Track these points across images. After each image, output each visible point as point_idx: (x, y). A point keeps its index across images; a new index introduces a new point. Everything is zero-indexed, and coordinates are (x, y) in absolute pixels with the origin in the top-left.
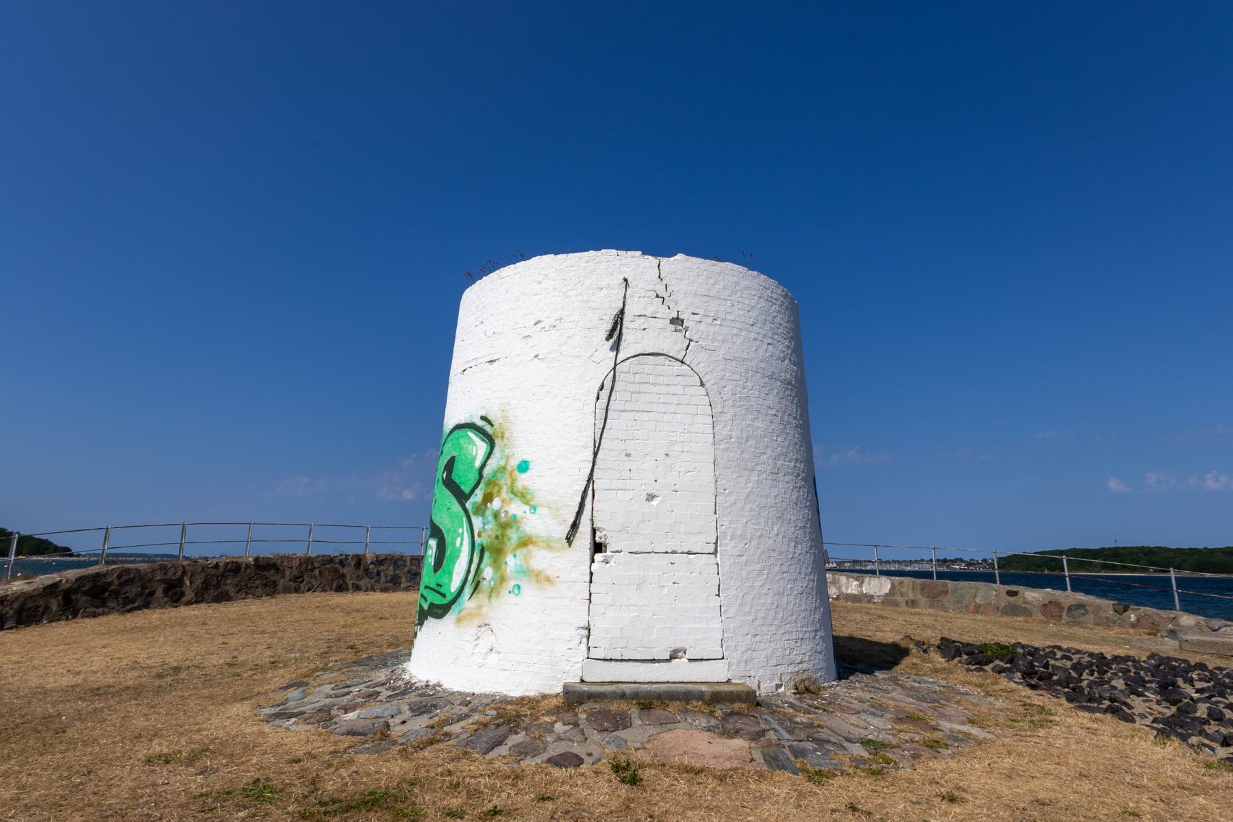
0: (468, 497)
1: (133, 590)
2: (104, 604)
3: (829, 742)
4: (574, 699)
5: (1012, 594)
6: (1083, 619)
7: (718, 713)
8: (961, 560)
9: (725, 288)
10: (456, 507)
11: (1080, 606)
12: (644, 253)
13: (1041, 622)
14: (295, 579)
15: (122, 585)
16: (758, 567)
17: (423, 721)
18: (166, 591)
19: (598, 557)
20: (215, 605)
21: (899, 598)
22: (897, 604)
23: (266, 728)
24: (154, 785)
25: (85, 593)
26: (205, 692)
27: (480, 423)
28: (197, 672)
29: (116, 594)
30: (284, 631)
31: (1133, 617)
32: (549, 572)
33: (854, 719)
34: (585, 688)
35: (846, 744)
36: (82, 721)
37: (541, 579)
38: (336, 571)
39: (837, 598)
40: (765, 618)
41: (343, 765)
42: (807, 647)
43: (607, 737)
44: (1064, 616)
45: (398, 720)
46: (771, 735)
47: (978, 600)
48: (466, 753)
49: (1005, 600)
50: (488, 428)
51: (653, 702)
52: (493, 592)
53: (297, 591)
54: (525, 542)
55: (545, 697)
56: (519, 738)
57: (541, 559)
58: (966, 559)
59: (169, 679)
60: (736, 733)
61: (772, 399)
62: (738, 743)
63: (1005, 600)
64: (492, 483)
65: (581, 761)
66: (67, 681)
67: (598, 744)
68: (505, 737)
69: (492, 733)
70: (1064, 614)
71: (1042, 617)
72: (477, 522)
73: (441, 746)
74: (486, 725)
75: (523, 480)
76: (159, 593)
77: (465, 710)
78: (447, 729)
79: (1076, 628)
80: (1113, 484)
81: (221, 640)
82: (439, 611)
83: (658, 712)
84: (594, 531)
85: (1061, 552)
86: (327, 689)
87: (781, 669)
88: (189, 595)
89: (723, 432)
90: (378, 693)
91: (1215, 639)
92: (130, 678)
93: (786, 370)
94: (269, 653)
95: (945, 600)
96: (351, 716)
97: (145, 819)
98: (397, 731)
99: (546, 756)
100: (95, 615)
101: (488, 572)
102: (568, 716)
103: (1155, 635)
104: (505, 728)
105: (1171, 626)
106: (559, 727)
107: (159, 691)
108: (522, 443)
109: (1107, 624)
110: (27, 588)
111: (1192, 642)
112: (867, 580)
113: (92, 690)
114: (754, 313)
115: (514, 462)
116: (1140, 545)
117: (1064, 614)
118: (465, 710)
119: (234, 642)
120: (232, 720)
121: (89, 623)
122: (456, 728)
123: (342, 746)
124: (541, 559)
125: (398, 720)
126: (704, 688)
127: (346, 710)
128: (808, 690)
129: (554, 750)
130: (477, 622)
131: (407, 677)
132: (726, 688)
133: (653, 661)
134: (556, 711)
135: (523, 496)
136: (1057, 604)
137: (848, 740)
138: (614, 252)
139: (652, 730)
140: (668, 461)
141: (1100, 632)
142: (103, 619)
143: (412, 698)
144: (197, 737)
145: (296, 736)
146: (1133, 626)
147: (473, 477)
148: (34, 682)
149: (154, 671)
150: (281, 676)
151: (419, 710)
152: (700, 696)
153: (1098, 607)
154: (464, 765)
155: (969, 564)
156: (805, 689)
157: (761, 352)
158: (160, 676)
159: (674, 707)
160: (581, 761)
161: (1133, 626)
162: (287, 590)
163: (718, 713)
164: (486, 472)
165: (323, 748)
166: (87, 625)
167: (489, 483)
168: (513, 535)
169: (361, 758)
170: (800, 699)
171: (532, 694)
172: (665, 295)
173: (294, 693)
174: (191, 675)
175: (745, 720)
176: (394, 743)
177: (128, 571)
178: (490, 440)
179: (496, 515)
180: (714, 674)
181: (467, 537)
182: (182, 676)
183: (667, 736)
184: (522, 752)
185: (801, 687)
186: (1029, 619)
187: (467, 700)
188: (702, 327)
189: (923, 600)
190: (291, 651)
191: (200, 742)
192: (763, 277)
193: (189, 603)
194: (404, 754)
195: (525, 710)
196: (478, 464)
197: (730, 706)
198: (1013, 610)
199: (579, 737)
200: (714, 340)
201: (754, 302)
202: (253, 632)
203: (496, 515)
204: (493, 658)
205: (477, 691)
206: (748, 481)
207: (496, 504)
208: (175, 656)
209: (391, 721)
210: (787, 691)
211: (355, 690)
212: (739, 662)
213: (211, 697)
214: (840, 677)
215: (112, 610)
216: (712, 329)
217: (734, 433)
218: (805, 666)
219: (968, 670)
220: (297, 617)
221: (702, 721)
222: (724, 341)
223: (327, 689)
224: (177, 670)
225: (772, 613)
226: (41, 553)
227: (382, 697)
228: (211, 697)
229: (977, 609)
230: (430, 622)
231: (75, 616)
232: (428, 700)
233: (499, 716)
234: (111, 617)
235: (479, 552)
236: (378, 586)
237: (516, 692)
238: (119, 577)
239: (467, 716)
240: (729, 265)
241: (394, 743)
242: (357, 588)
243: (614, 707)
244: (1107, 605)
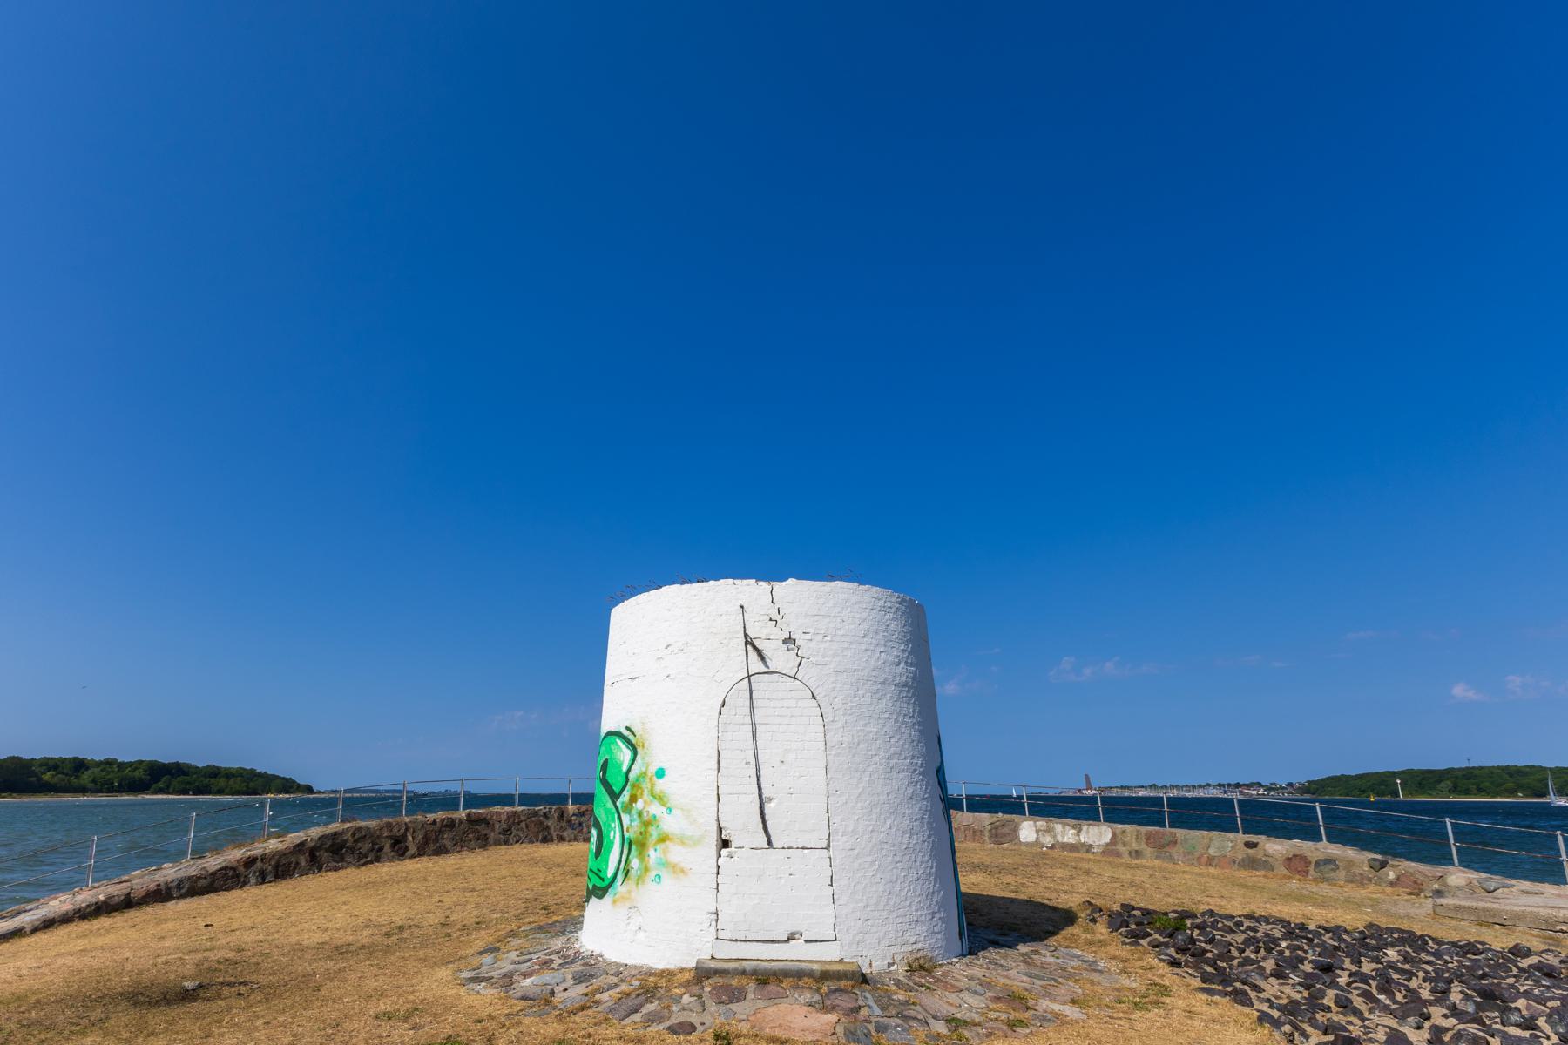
0: (618, 797)
1: (365, 847)
2: (342, 859)
3: (915, 1018)
4: (702, 974)
5: (1249, 845)
6: (1333, 875)
7: (825, 989)
8: (1259, 785)
9: (835, 606)
10: (610, 805)
11: (1330, 861)
12: (758, 579)
13: (1284, 877)
14: (504, 832)
15: (356, 842)
16: (869, 859)
18: (393, 846)
19: (724, 852)
20: (435, 858)
21: (1120, 848)
22: (1118, 855)
23: (462, 991)
24: (380, 1037)
25: (327, 850)
26: (421, 953)
27: (626, 733)
28: (416, 931)
29: (352, 850)
30: (490, 889)
31: (1392, 875)
32: (683, 865)
33: (952, 998)
34: (713, 965)
35: (931, 1021)
36: (331, 980)
37: (677, 870)
38: (541, 823)
39: (1053, 847)
40: (877, 904)
41: (513, 1025)
42: (922, 929)
43: (722, 1008)
44: (1312, 872)
46: (864, 1012)
47: (1211, 851)
48: (607, 1019)
49: (1242, 853)
50: (631, 737)
51: (768, 978)
52: (639, 879)
53: (506, 843)
54: (663, 839)
55: (682, 970)
57: (676, 853)
58: (1266, 782)
59: (394, 938)
60: (833, 1008)
61: (885, 703)
62: (831, 1018)
63: (1242, 853)
64: (635, 786)
66: (317, 938)
67: (712, 1015)
68: (641, 1006)
69: (632, 1002)
70: (1312, 868)
71: (1285, 872)
72: (625, 818)
73: (590, 1012)
74: (628, 995)
75: (661, 785)
76: (387, 848)
77: (616, 980)
78: (598, 997)
79: (1324, 886)
80: (1459, 691)
81: (437, 898)
82: (600, 892)
83: (772, 988)
84: (720, 829)
85: (1394, 774)
86: (513, 955)
87: (893, 949)
88: (413, 850)
89: (833, 738)
90: (552, 961)
91: (1475, 904)
92: (365, 937)
93: (902, 673)
94: (476, 913)
95: (1174, 851)
96: (528, 981)
97: (402, 1032)
98: (560, 996)
99: (668, 1024)
101: (635, 863)
102: (695, 989)
103: (1418, 895)
105: (1436, 886)
106: (686, 999)
107: (387, 950)
108: (657, 754)
109: (1361, 881)
110: (281, 847)
111: (1447, 907)
112: (1085, 828)
113: (337, 948)
114: (865, 626)
115: (652, 770)
116: (1521, 762)
117: (1312, 868)
118: (616, 980)
119: (449, 900)
120: (437, 983)
121: (332, 876)
122: (604, 997)
123: (516, 1009)
124: (676, 853)
125: (561, 988)
126: (816, 967)
127: (525, 976)
128: (922, 967)
129: (675, 1020)
131: (577, 946)
132: (835, 967)
133: (773, 942)
135: (660, 799)
136: (1303, 859)
137: (935, 1017)
138: (731, 581)
139: (760, 1004)
140: (784, 767)
141: (1352, 891)
143: (577, 967)
144: (411, 997)
145: (484, 998)
146: (1392, 884)
147: (622, 780)
148: (294, 939)
149: (384, 929)
151: (580, 979)
152: (811, 974)
154: (601, 1030)
155: (1269, 789)
156: (920, 967)
157: (872, 661)
158: (388, 935)
159: (787, 983)
160: (694, 1028)
161: (1392, 884)
162: (498, 843)
163: (825, 989)
164: (631, 776)
165: (500, 1010)
166: (330, 879)
167: (635, 786)
168: (654, 833)
169: (527, 1021)
170: (909, 978)
171: (672, 967)
172: (778, 618)
173: (487, 959)
174: (411, 934)
176: (555, 1008)
177: (360, 829)
178: (634, 748)
179: (640, 814)
181: (618, 830)
182: (405, 935)
183: (770, 1010)
184: (652, 1019)
185: (916, 965)
186: (1270, 874)
187: (619, 971)
188: (812, 645)
189: (1148, 851)
190: (493, 911)
191: (414, 1002)
192: (875, 589)
193: (413, 857)
194: (560, 1018)
195: (662, 983)
196: (625, 769)
197: (839, 984)
198: (1252, 864)
199: (699, 1008)
200: (824, 656)
201: (864, 615)
202: (465, 890)
203: (640, 814)
204: (641, 935)
207: (639, 805)
208: (400, 915)
209: (556, 989)
210: (900, 970)
211: (534, 956)
212: (850, 944)
213: (425, 960)
214: (972, 952)
216: (823, 646)
217: (846, 739)
218: (919, 946)
219: (1124, 943)
220: (504, 873)
221: (807, 996)
222: (834, 656)
223: (513, 955)
224: (401, 928)
225: (884, 900)
226: (287, 792)
227: (554, 965)
228: (425, 960)
229: (1210, 861)
230: (594, 900)
231: (320, 870)
232: (589, 970)
234: (349, 871)
235: (628, 844)
236: (580, 837)
237: (660, 965)
238: (353, 835)
239: (616, 985)
241: (555, 1008)
242: (561, 839)
243: (735, 982)
244: (1360, 858)
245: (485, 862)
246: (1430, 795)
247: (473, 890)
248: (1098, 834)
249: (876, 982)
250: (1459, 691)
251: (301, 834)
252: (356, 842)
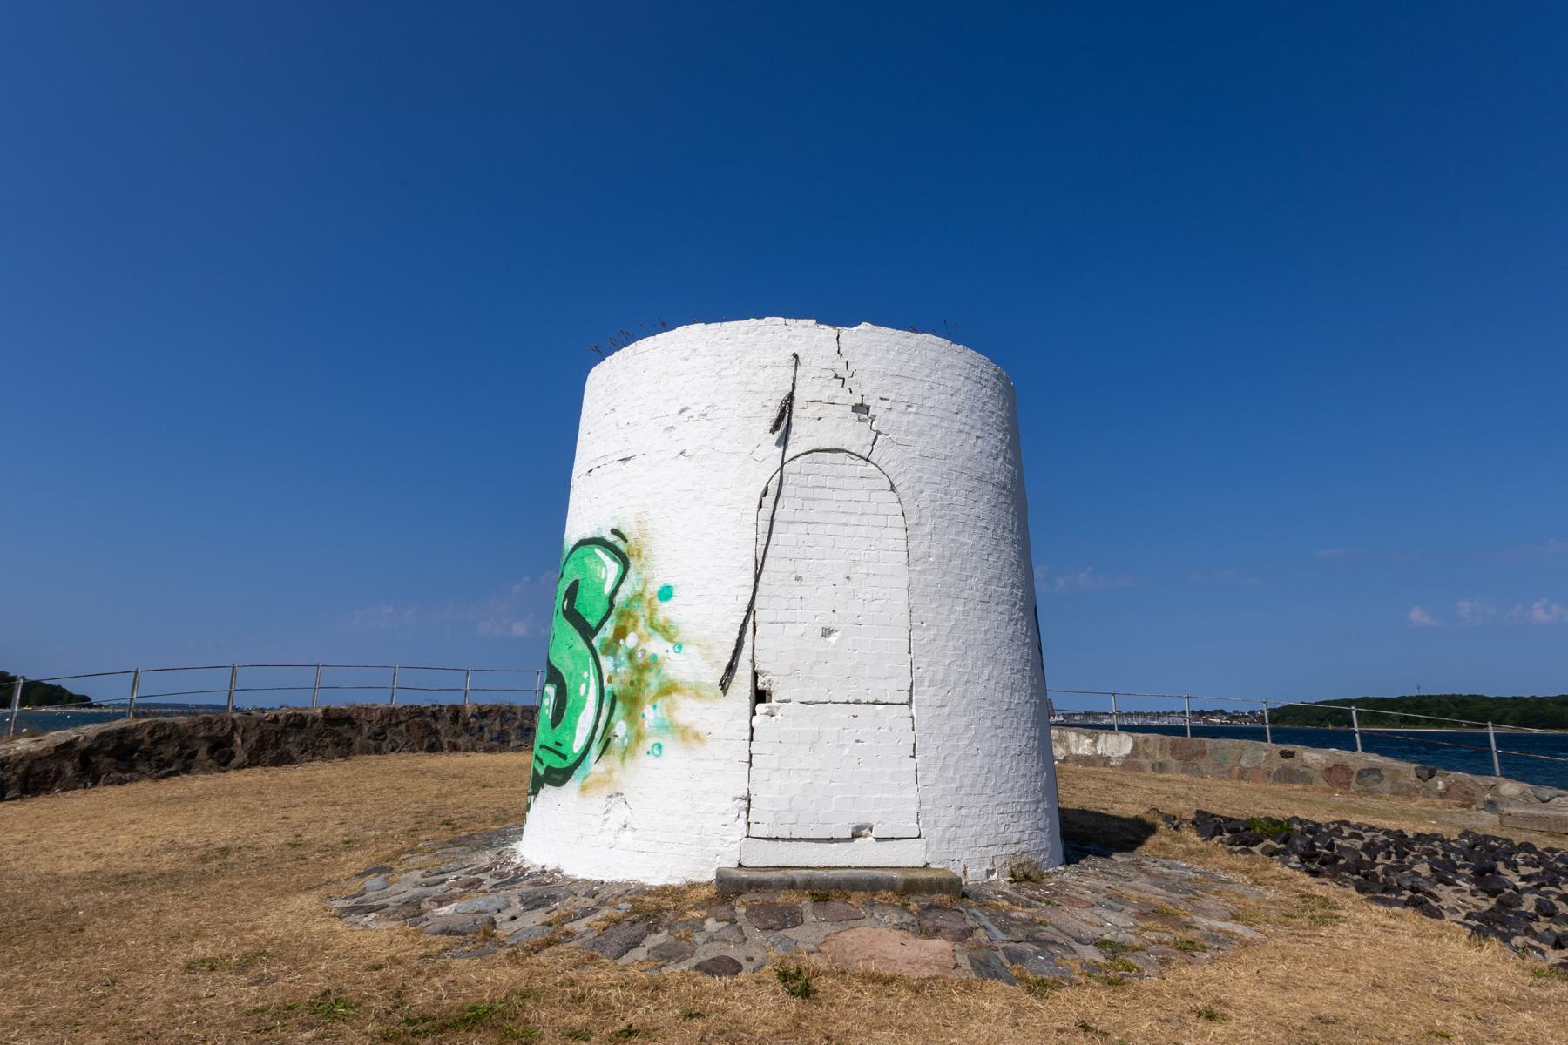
0: (595, 632)
1: (169, 751)
2: (132, 768)
3: (1054, 943)
4: (729, 888)
5: (1286, 755)
6: (1377, 786)
7: (914, 906)
8: (1223, 712)
9: (922, 366)
10: (580, 645)
11: (1374, 770)
12: (819, 322)
13: (1324, 790)
14: (375, 736)
15: (155, 743)
16: (964, 721)
17: (539, 916)
18: (211, 752)
19: (761, 708)
20: (274, 770)
21: (1142, 760)
22: (1140, 768)
23: (339, 926)
24: (196, 998)
25: (108, 754)
27: (611, 538)
28: (250, 855)
29: (148, 755)
30: (361, 802)
32: (698, 728)
33: (1086, 914)
34: (744, 874)
35: (1076, 946)
36: (105, 916)
37: (688, 736)
38: (428, 725)
39: (1065, 761)
40: (973, 785)
41: (436, 972)
42: (1026, 822)
43: (773, 937)
44: (1354, 783)
45: (506, 915)
46: (981, 935)
47: (1243, 763)
48: (592, 957)
49: (1278, 763)
50: (620, 544)
51: (830, 892)
52: (627, 752)
53: (378, 751)
54: (668, 690)
56: (660, 938)
57: (687, 711)
58: (1229, 710)
59: (214, 864)
60: (936, 932)
61: (982, 508)
62: (939, 944)
63: (1278, 763)
64: (626, 614)
65: (739, 968)
66: (85, 865)
67: (760, 945)
68: (642, 937)
69: (626, 932)
70: (1354, 780)
71: (1325, 785)
72: (607, 663)
73: (561, 948)
74: (617, 922)
75: (665, 610)
76: (202, 754)
77: (591, 902)
78: (568, 926)
79: (1369, 799)
80: (1416, 616)
81: (281, 814)
82: (558, 777)
83: (836, 905)
84: (755, 675)
85: (1349, 702)
86: (416, 876)
87: (994, 851)
88: (241, 756)
89: (919, 549)
90: (481, 881)
91: (1545, 813)
92: (166, 862)
93: (1000, 470)
94: (342, 830)
96: (447, 910)
97: (185, 1041)
98: (504, 929)
99: (694, 961)
100: (121, 782)
101: (620, 727)
102: (723, 911)
103: (1469, 807)
104: (642, 926)
105: (1489, 796)
106: (711, 925)
107: (202, 878)
108: (663, 563)
109: (1408, 793)
110: (34, 747)
111: (1516, 817)
112: (1102, 737)
113: (117, 877)
114: (959, 398)
115: (654, 588)
117: (1354, 780)
119: (297, 816)
120: (295, 915)
121: (113, 792)
122: (580, 926)
123: (435, 949)
124: (687, 711)
125: (506, 915)
126: (895, 875)
127: (440, 902)
128: (1027, 877)
130: (606, 791)
131: (517, 861)
132: (923, 875)
133: (831, 840)
134: (707, 904)
135: (665, 631)
136: (1344, 768)
137: (1079, 941)
138: (781, 320)
139: (829, 928)
140: (850, 586)
141: (1399, 803)
142: (131, 787)
143: (524, 887)
144: (250, 937)
145: (377, 935)
146: (1441, 795)
147: (602, 606)
148: (44, 868)
149: (196, 854)
150: (358, 860)
151: (533, 903)
152: (890, 885)
153: (1397, 772)
154: (590, 972)
155: (1232, 717)
156: (1024, 876)
157: (967, 448)
158: (203, 859)
159: (857, 898)
160: (739, 968)
161: (1441, 795)
162: (365, 751)
163: (914, 906)
164: (618, 599)
165: (411, 951)
167: (622, 614)
168: (653, 680)
169: (459, 964)
170: (1017, 889)
171: (676, 882)
172: (846, 375)
173: (374, 882)
174: (242, 858)
175: (947, 915)
176: (501, 944)
177: (162, 726)
178: (624, 560)
179: (631, 655)
180: (908, 856)
182: (231, 859)
183: (848, 936)
184: (664, 956)
185: (1019, 873)
186: (1309, 787)
187: (593, 890)
188: (893, 415)
189: (1173, 763)
190: (370, 828)
191: (254, 944)
192: (970, 352)
193: (240, 767)
194: (514, 958)
195: (668, 903)
196: (607, 590)
197: (928, 898)
198: (1288, 776)
199: (737, 937)
200: (907, 433)
201: (959, 384)
202: (322, 804)
203: (631, 655)
204: (627, 836)
206: (951, 611)
207: (631, 641)
208: (223, 834)
209: (497, 917)
210: (1000, 879)
211: (452, 877)
212: (940, 842)
213: (269, 887)
214: (1068, 860)
215: (142, 776)
216: (906, 419)
217: (934, 551)
218: (1024, 846)
219: (1231, 852)
220: (377, 784)
221: (893, 917)
222: (921, 434)
223: (416, 876)
224: (225, 851)
225: (982, 779)
227: (486, 886)
228: (269, 887)
229: (1243, 775)
230: (547, 791)
231: (95, 783)
232: (544, 890)
233: (635, 910)
234: (141, 784)
235: (609, 701)
236: (480, 745)
238: (152, 733)
239: (594, 910)
240: (927, 337)
241: (501, 944)
242: (454, 748)
243: (780, 899)
244: (1407, 770)
245: (347, 773)
246: (1384, 725)
247: (334, 804)
248: (1117, 746)
249: (977, 897)
250: (1416, 616)
251: (69, 732)
252: (155, 743)
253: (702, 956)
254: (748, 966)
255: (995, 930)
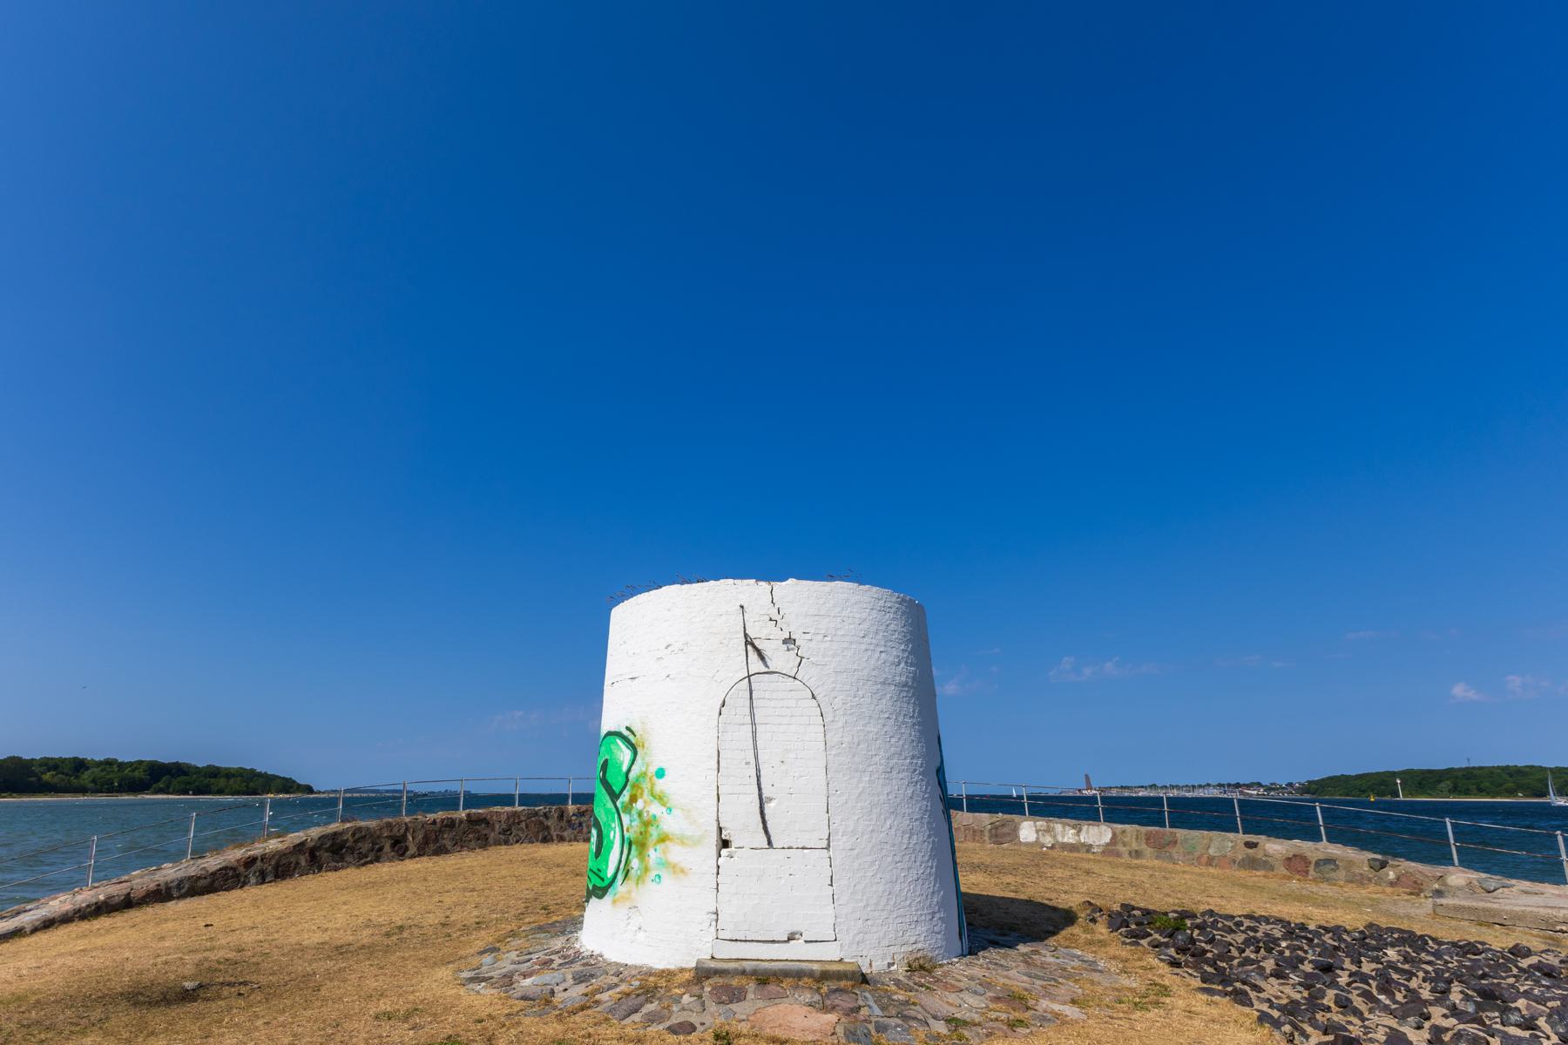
0: (618, 797)
1: (365, 847)
2: (342, 859)
3: (915, 1018)
4: (702, 974)
6: (1333, 875)
7: (825, 989)
8: (1259, 785)
10: (610, 805)
11: (1330, 861)
13: (1284, 877)
14: (504, 832)
15: (356, 842)
16: (869, 859)
17: (582, 989)
18: (393, 846)
19: (724, 852)
20: (435, 858)
21: (1120, 848)
22: (1118, 855)
23: (462, 991)
24: (380, 1037)
25: (327, 850)
26: (421, 953)
27: (626, 733)
28: (416, 931)
29: (352, 850)
30: (490, 889)
31: (1392, 875)
33: (952, 998)
34: (713, 965)
35: (931, 1021)
36: (331, 980)
37: (677, 870)
39: (1053, 847)
40: (877, 904)
43: (722, 1008)
44: (1312, 872)
45: (561, 988)
46: (864, 1012)
47: (1211, 852)
48: (607, 1019)
49: (1243, 853)
50: (631, 737)
51: (768, 978)
52: (639, 879)
53: (506, 843)
54: (663, 839)
55: (682, 970)
56: (650, 1007)
57: (676, 853)
58: (1266, 782)
59: (394, 938)
60: (833, 1008)
61: (885, 703)
62: (832, 1018)
63: (1243, 853)
64: (635, 786)
65: (694, 1029)
66: (318, 938)
68: (642, 1006)
69: (632, 1002)
70: (1312, 868)
71: (1285, 872)
72: (625, 818)
73: (590, 1012)
74: (628, 995)
75: (661, 785)
76: (387, 848)
77: (616, 980)
78: (598, 997)
81: (436, 898)
82: (600, 892)
83: (772, 988)
84: (720, 829)
85: (1394, 775)
86: (513, 955)
87: (893, 949)
88: (413, 850)
89: (833, 738)
90: (552, 961)
91: (1475, 904)
92: (365, 937)
93: (902, 673)
94: (476, 913)
95: (1174, 851)
96: (528, 981)
98: (559, 997)
99: (668, 1024)
100: (336, 869)
101: (635, 863)
102: (695, 990)
103: (1418, 895)
104: (642, 998)
106: (686, 999)
107: (387, 950)
108: (657, 754)
109: (1361, 881)
110: (281, 847)
111: (1447, 907)
112: (1085, 828)
113: (337, 948)
114: (865, 626)
115: (652, 770)
116: (1521, 762)
117: (1312, 868)
118: (616, 980)
119: (448, 900)
120: (437, 983)
121: (332, 875)
122: (604, 997)
123: (516, 1009)
124: (676, 853)
125: (561, 988)
126: (816, 967)
127: (525, 976)
130: (628, 904)
131: (577, 946)
132: (835, 967)
133: (773, 942)
134: (687, 984)
135: (660, 799)
136: (1303, 859)
137: (935, 1017)
138: (731, 581)
139: (760, 1004)
140: (784, 767)
142: (343, 873)
143: (577, 967)
144: (411, 998)
145: (484, 998)
146: (1392, 884)
147: (622, 780)
148: (293, 940)
149: (384, 929)
150: (484, 938)
151: (580, 979)
152: (811, 974)
153: (1351, 863)
154: (601, 1030)
155: (1269, 789)
156: (920, 967)
157: (872, 662)
158: (388, 935)
159: (787, 982)
160: (694, 1029)
161: (1392, 884)
162: (498, 843)
163: (825, 989)
164: (631, 776)
165: (500, 1010)
167: (635, 786)
168: (654, 833)
169: (527, 1021)
170: (909, 978)
171: (672, 967)
172: (778, 617)
173: (487, 959)
174: (411, 934)
175: (845, 997)
176: (555, 1008)
177: (360, 829)
178: (634, 748)
179: (640, 814)
180: (828, 953)
181: (618, 830)
182: (405, 935)
183: (770, 1010)
184: (652, 1019)
185: (916, 965)
186: (1270, 874)
187: (620, 971)
189: (1148, 851)
190: (493, 911)
191: (414, 1002)
192: (875, 589)
193: (413, 857)
194: (560, 1018)
196: (625, 769)
197: (839, 984)
198: (1252, 864)
199: (699, 1008)
200: (824, 656)
201: (864, 615)
202: (465, 890)
203: (640, 814)
204: (641, 935)
205: (629, 963)
206: (860, 781)
207: (639, 805)
208: (400, 915)
209: (556, 989)
210: (900, 970)
211: (534, 956)
212: (850, 944)
213: (425, 960)
214: (972, 952)
215: (349, 865)
217: (846, 739)
218: (919, 946)
219: (1124, 943)
220: (504, 873)
221: (807, 996)
222: (834, 656)
223: (513, 955)
224: (401, 928)
225: (884, 900)
226: (287, 792)
227: (554, 965)
228: (425, 960)
229: (1210, 862)
230: (594, 900)
231: (320, 870)
232: (589, 970)
233: (641, 987)
235: (628, 844)
236: (580, 837)
237: (660, 965)
238: (353, 835)
239: (616, 985)
240: (838, 584)
241: (555, 1008)
242: (561, 839)
243: (735, 982)
244: (1360, 858)
245: (485, 862)
247: (473, 890)
248: (1098, 834)
250: (1459, 690)
251: (301, 834)
252: (356, 842)
253: (674, 1021)
254: (700, 1028)
255: (875, 1007)
